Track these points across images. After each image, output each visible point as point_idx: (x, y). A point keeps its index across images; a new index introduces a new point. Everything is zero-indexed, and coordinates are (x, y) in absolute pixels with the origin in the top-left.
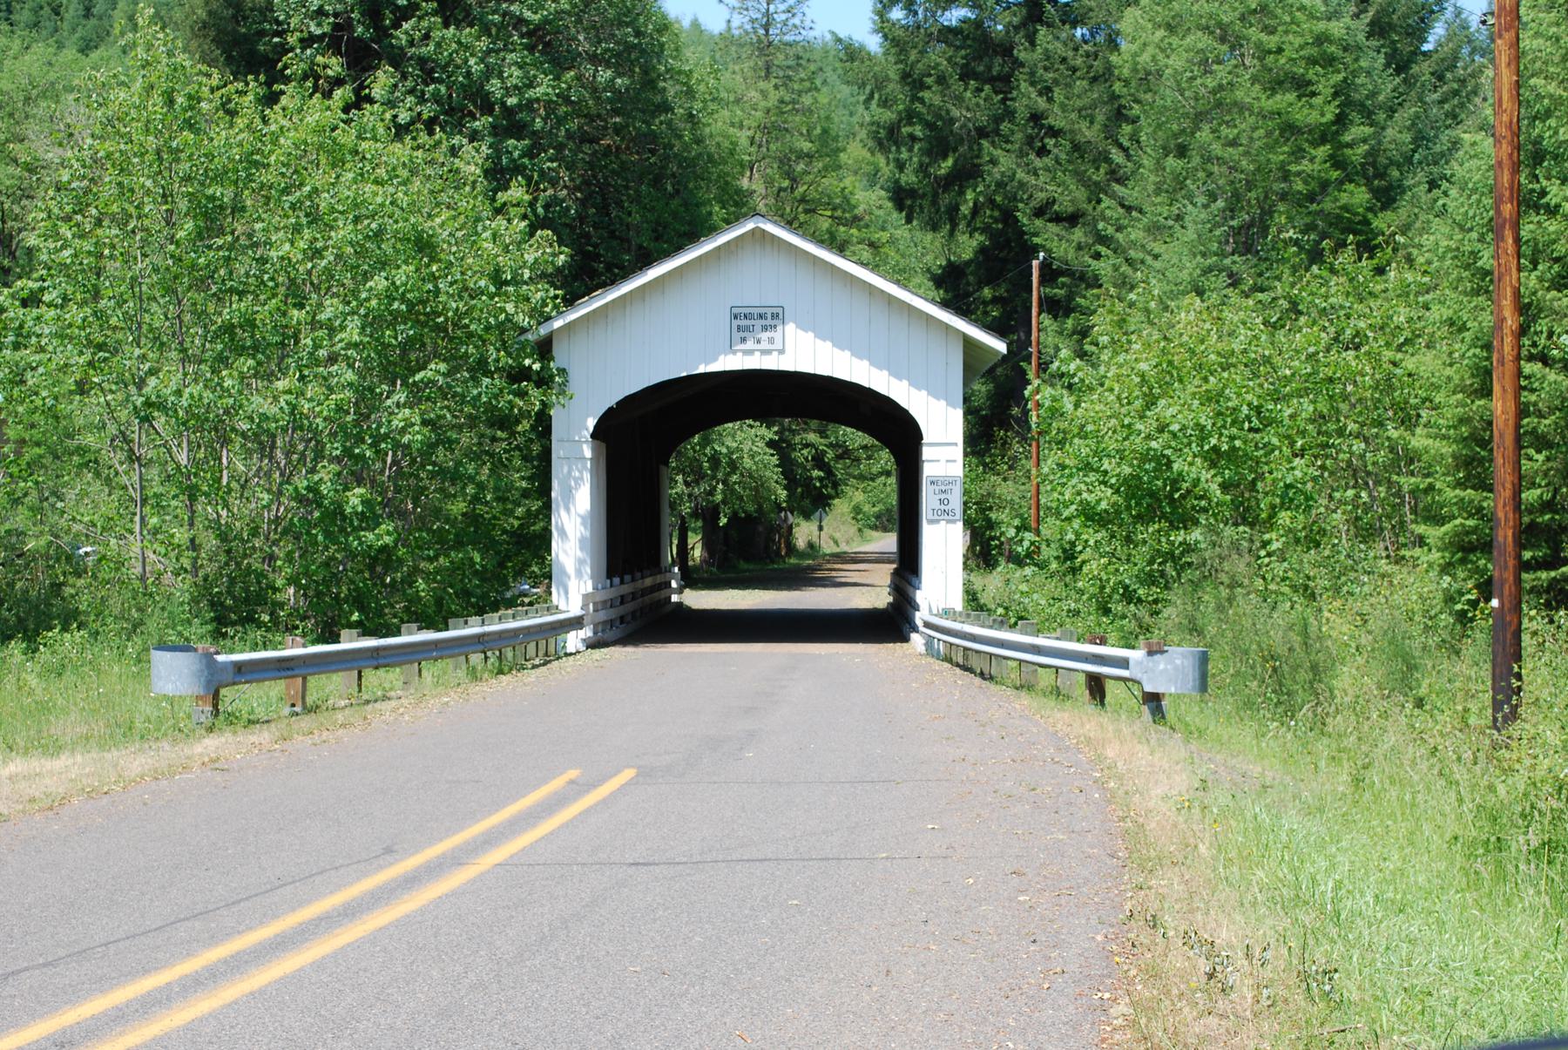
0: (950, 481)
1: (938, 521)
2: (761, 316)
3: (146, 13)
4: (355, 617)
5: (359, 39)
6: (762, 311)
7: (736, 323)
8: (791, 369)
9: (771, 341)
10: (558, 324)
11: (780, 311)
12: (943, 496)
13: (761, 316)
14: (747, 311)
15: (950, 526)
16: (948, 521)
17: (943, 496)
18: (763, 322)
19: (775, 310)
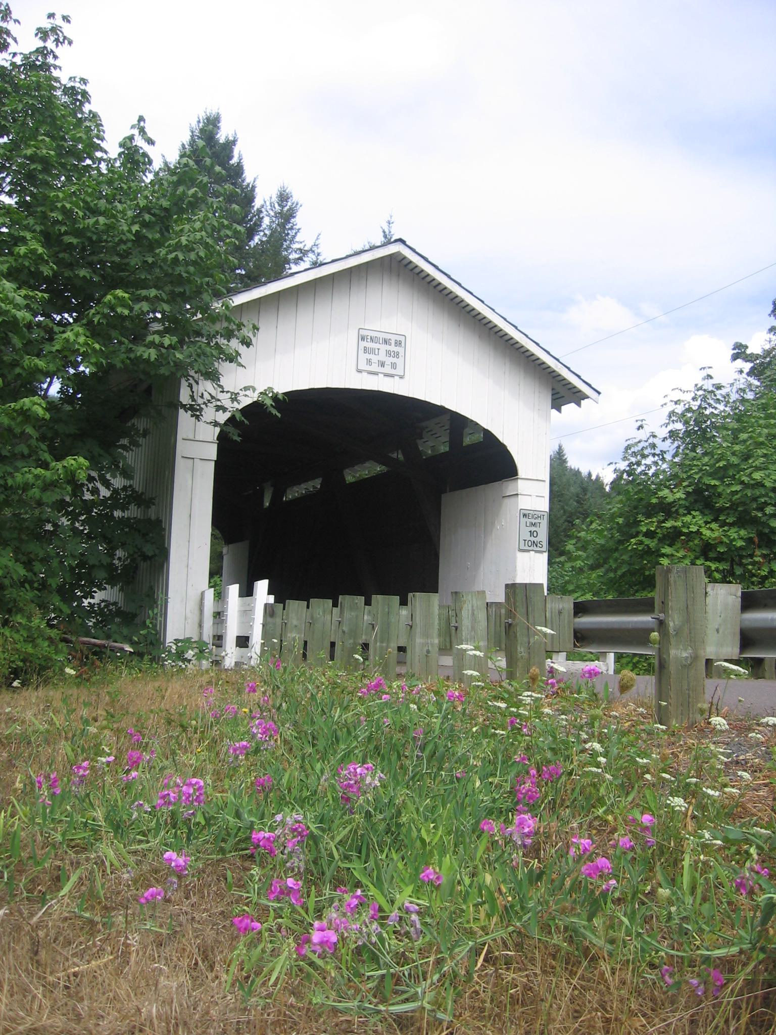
0: (536, 515)
1: (528, 551)
2: (386, 342)
3: (538, 1033)
4: (79, 360)
5: (114, 564)
6: (388, 336)
7: (363, 344)
8: (423, 399)
9: (394, 366)
10: (239, 299)
11: (402, 339)
12: (533, 529)
13: (386, 342)
14: (374, 334)
15: (538, 555)
16: (536, 552)
17: (533, 529)
18: (388, 347)
19: (399, 338)
